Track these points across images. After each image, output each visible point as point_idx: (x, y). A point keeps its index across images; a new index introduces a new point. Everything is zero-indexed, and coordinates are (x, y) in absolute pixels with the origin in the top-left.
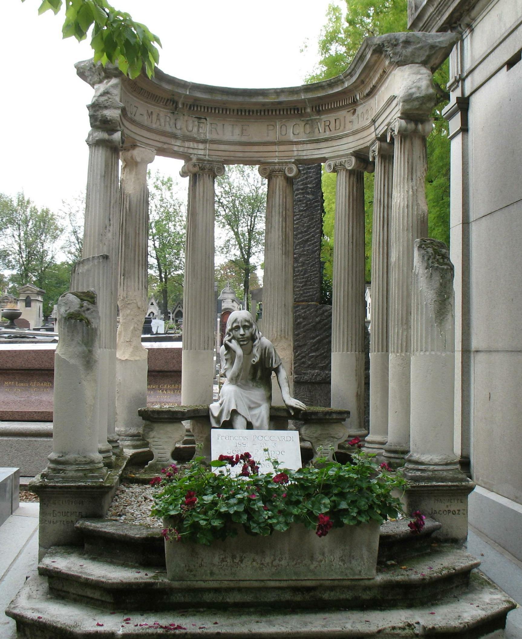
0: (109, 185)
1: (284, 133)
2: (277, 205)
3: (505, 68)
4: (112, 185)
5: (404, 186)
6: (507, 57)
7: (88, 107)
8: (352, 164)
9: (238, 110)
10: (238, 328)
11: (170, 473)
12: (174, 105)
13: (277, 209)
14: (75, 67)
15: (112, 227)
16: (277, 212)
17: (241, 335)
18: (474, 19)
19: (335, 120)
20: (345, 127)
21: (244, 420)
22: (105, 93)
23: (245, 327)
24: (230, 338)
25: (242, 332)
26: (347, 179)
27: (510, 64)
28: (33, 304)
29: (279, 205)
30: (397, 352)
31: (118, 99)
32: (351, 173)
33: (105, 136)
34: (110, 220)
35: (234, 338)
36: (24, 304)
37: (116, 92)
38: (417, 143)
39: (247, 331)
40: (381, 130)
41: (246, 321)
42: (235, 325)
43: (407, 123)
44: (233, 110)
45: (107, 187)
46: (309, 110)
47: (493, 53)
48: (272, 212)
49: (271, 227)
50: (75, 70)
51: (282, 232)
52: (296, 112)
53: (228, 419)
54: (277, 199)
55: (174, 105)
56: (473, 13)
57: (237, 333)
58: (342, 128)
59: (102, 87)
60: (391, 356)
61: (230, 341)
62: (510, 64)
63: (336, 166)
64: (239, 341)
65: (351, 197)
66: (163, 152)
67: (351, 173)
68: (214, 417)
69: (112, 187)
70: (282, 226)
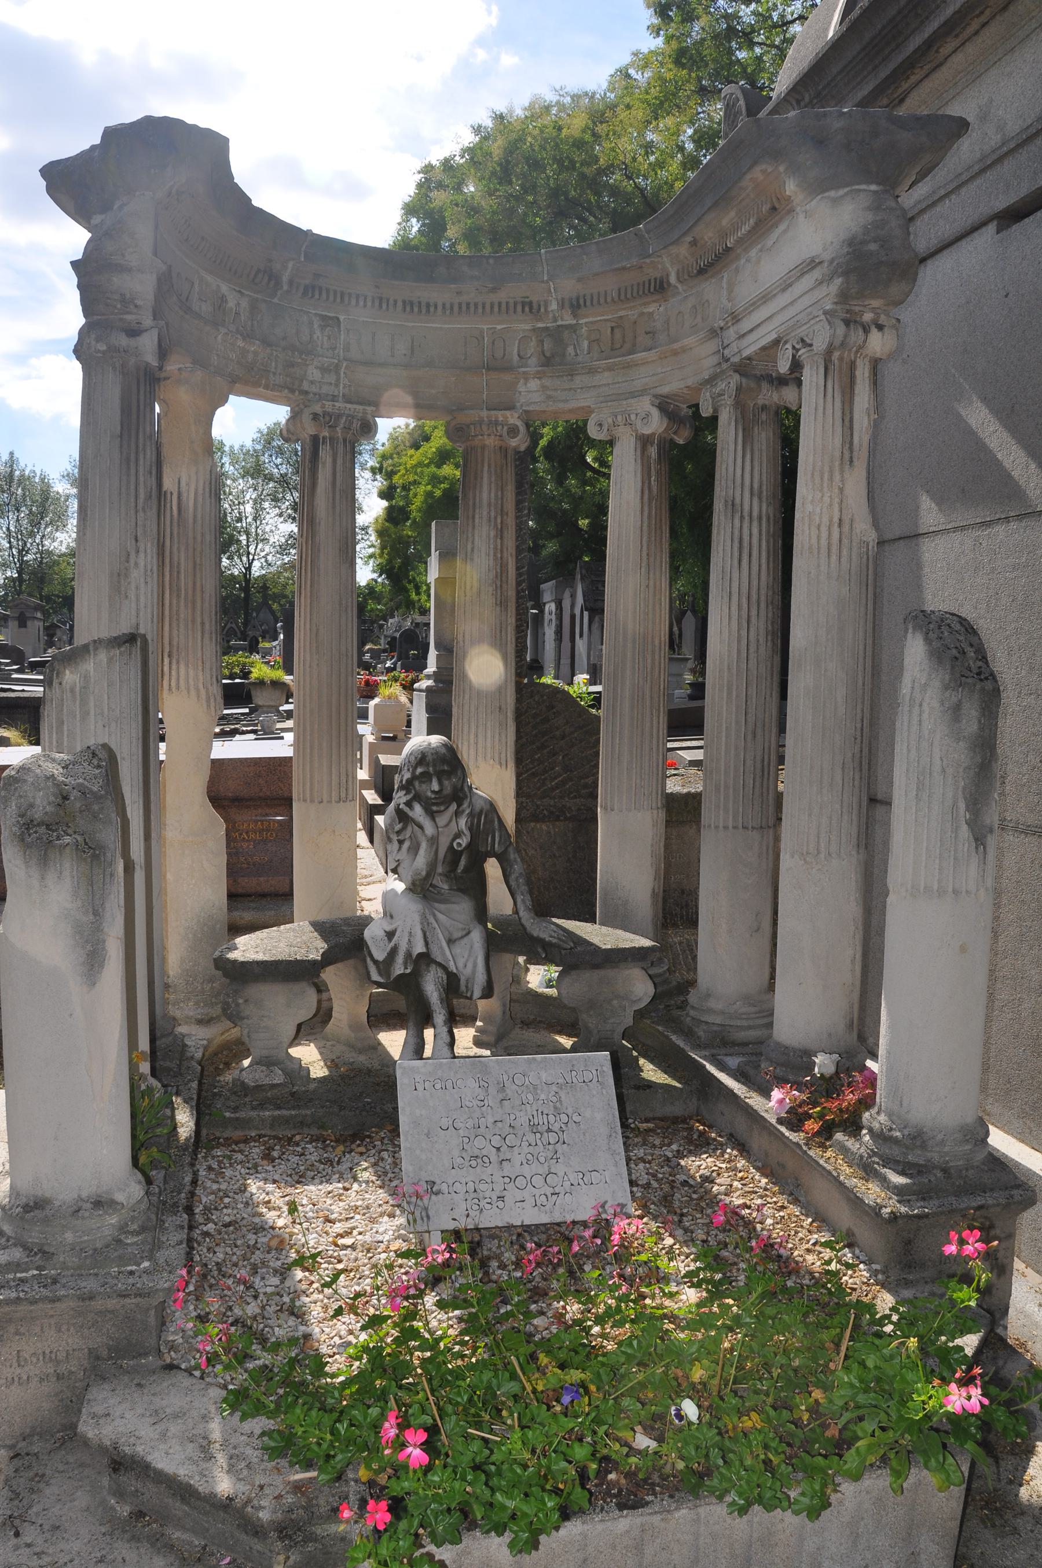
0: (133, 456)
2: (485, 502)
3: (992, 228)
4: (141, 456)
5: (831, 479)
6: (1001, 203)
7: (75, 264)
12: (272, 283)
13: (485, 513)
15: (142, 555)
16: (485, 519)
17: (433, 792)
19: (612, 328)
21: (440, 973)
24: (409, 797)
26: (639, 453)
27: (1011, 216)
28: (29, 623)
29: (489, 505)
34: (137, 541)
35: (417, 798)
36: (16, 623)
39: (446, 783)
42: (419, 770)
44: (395, 302)
45: (128, 460)
48: (474, 517)
49: (473, 550)
51: (495, 559)
53: (408, 971)
54: (485, 495)
55: (272, 283)
57: (424, 786)
61: (409, 804)
62: (1011, 216)
65: (646, 492)
68: (376, 962)
69: (141, 462)
70: (495, 548)
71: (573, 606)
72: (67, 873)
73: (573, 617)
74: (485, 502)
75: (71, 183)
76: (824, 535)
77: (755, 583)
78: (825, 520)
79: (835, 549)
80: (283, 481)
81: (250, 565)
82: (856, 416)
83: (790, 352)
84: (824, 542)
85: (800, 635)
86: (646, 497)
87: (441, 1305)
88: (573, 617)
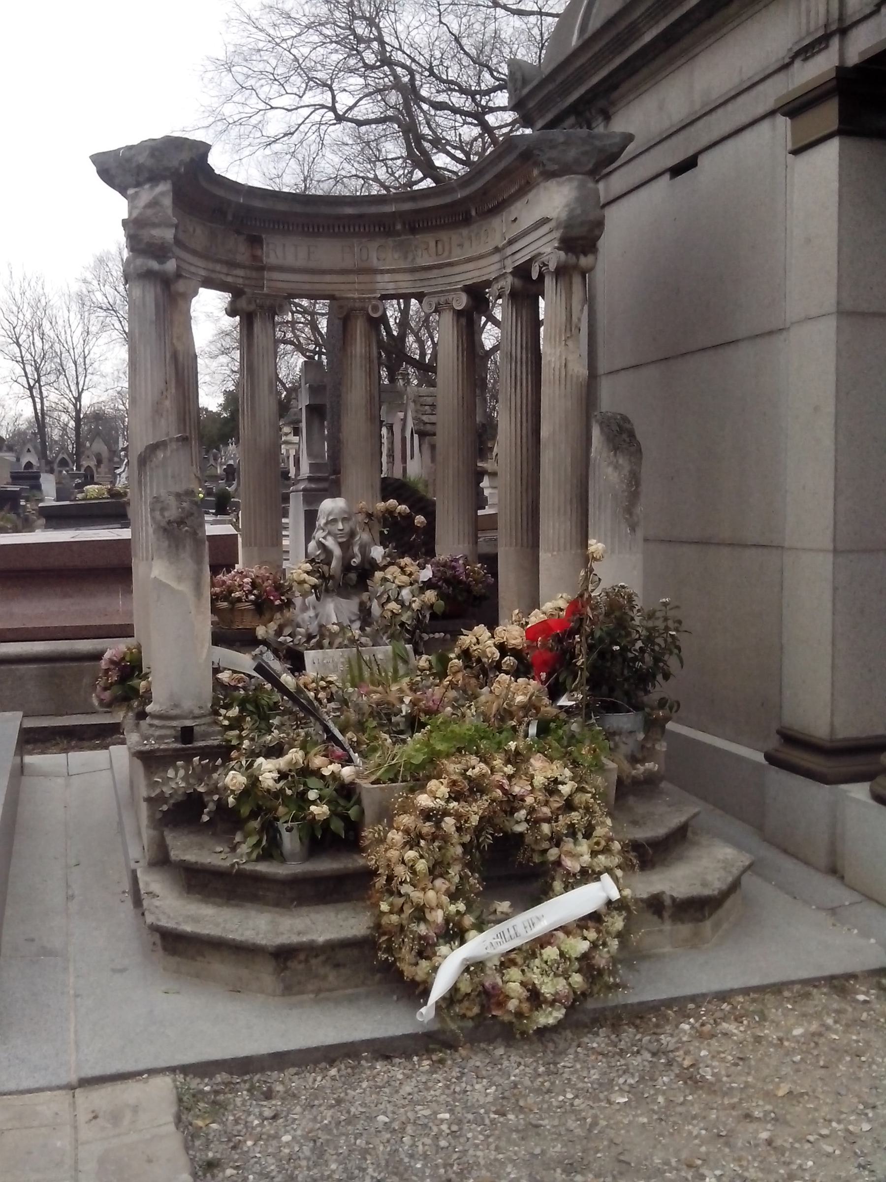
1: (365, 258)
2: (358, 355)
8: (461, 301)
9: (303, 225)
10: (335, 521)
11: (409, 755)
14: (94, 162)
18: (613, 104)
20: (450, 252)
22: (154, 203)
23: (344, 520)
24: (325, 534)
25: (340, 526)
30: (554, 551)
31: (170, 212)
32: (459, 314)
33: (154, 265)
35: (329, 533)
37: (167, 202)
38: (577, 280)
40: (522, 258)
41: (345, 512)
43: (566, 254)
46: (399, 227)
47: (647, 154)
50: (94, 169)
52: (382, 229)
56: (615, 95)
58: (446, 253)
59: (146, 195)
60: (544, 556)
63: (439, 304)
64: (335, 536)
66: (209, 283)
67: (459, 314)
71: (403, 430)
72: (188, 547)
73: (404, 439)
74: (358, 355)
75: (116, 169)
76: (557, 373)
77: (524, 401)
78: (558, 366)
79: (563, 382)
80: (111, 309)
81: (80, 394)
82: (573, 305)
83: (538, 268)
84: (557, 377)
85: (545, 431)
86: (460, 348)
87: (388, 638)
88: (404, 439)
